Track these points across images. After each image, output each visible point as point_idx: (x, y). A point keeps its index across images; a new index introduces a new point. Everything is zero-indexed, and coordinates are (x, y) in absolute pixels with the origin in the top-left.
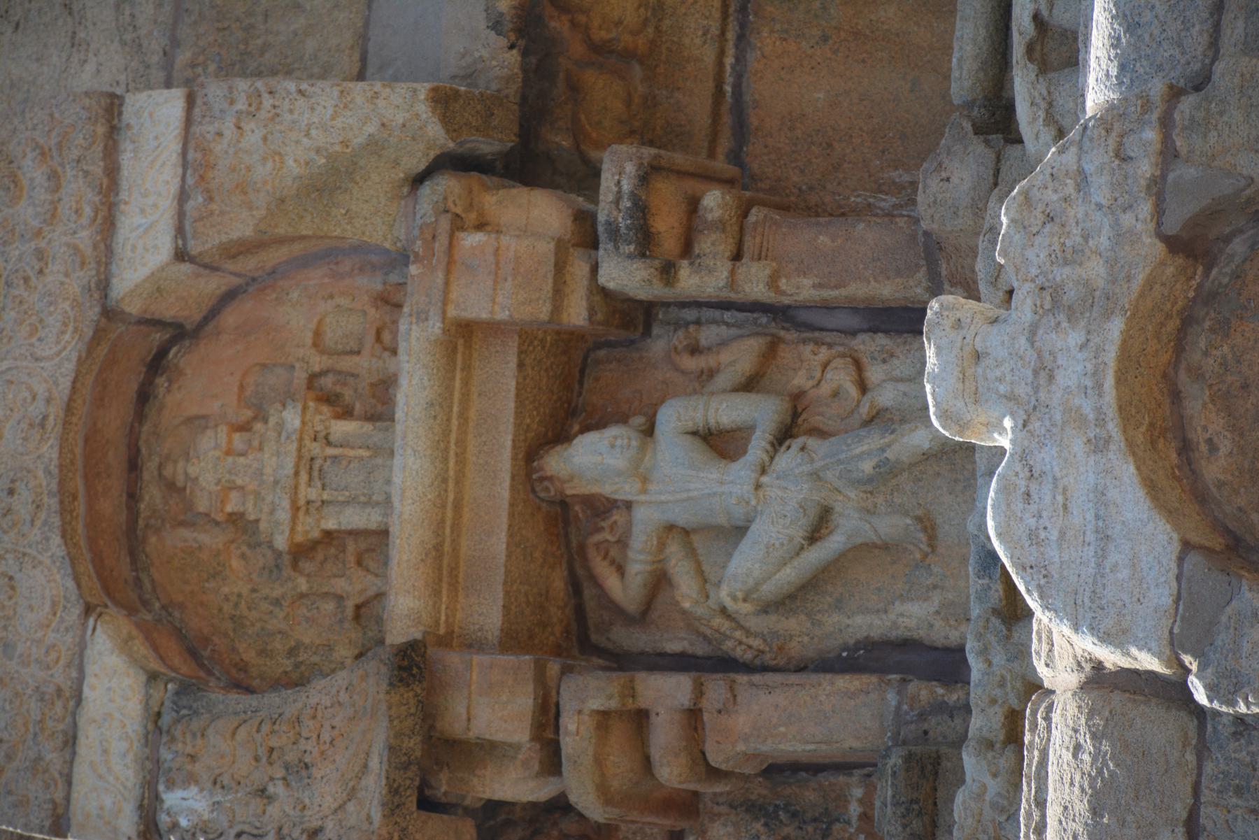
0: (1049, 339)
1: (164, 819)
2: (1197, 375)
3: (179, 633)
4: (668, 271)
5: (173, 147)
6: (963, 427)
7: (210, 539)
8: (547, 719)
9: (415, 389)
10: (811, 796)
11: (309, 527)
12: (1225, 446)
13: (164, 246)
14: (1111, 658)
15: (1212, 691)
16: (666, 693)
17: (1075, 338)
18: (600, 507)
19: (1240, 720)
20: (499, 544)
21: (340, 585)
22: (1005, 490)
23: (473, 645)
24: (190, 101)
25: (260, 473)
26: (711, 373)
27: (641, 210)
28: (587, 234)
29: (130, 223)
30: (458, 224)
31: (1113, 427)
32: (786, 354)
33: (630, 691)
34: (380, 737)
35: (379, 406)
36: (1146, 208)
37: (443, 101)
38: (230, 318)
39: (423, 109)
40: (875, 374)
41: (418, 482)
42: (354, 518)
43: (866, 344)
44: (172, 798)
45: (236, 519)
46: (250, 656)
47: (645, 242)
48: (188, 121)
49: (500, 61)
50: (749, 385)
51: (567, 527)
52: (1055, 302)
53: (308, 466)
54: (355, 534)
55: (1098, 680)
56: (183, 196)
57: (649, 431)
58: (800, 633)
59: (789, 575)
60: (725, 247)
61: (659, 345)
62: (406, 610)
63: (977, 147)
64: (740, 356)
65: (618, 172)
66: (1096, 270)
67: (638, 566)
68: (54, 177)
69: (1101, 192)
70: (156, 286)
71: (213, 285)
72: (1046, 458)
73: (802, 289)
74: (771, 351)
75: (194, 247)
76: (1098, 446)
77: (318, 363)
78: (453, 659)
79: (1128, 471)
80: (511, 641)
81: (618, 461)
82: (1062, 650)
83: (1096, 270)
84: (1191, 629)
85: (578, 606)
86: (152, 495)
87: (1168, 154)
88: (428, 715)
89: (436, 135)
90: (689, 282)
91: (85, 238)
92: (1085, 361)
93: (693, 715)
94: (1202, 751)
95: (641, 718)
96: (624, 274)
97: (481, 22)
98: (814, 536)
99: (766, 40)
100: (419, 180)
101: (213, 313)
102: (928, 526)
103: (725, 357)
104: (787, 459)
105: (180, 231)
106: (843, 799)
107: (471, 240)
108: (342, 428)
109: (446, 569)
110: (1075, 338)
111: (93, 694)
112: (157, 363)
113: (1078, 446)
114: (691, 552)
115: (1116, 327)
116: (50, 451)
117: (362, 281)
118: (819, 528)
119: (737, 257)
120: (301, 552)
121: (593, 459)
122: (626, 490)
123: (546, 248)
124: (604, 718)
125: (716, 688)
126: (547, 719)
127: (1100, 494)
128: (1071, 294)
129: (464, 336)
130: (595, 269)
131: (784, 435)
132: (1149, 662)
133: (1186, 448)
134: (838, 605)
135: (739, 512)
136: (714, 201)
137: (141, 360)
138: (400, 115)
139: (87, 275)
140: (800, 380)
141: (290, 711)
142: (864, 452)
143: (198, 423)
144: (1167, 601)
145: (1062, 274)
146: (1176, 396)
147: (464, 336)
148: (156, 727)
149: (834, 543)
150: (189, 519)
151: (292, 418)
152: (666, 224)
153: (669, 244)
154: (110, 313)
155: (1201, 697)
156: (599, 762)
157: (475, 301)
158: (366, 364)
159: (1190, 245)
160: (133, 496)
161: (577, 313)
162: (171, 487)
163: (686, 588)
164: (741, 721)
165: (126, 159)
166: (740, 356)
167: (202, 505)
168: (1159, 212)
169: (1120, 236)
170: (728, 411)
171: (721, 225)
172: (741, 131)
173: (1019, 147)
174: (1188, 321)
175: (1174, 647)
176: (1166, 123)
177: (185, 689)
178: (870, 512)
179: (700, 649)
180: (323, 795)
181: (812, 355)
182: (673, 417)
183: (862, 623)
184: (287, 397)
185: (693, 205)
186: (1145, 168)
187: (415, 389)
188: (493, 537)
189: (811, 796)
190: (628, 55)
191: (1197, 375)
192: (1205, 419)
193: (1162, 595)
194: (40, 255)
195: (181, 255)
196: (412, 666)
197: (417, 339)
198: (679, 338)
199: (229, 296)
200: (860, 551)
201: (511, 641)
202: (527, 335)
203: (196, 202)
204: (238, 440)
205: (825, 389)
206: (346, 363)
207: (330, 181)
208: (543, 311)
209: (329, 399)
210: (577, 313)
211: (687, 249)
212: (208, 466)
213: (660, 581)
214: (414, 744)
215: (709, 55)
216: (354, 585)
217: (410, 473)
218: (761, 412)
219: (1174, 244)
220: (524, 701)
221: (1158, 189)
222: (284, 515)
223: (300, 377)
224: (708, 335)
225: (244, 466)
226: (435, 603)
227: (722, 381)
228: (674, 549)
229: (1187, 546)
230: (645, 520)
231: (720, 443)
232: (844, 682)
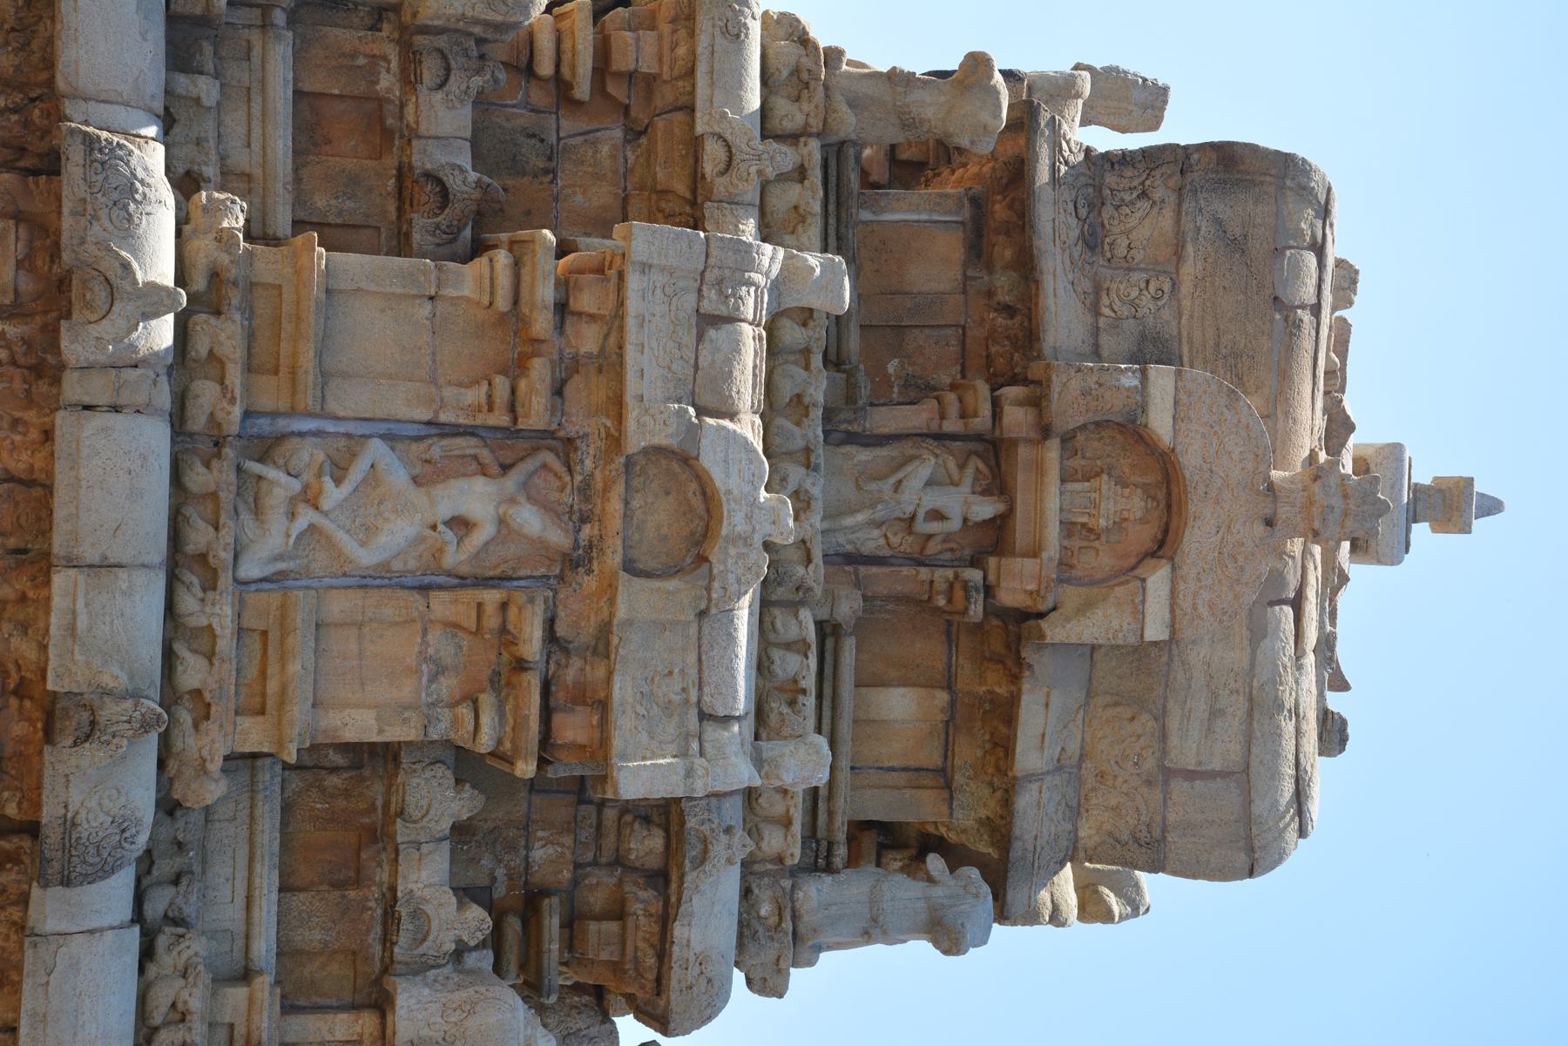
0: (748, 528)
1: (1138, 375)
2: (701, 518)
3: (1147, 445)
4: (956, 576)
5: (1148, 619)
6: (779, 500)
7: (1136, 479)
8: (997, 414)
9: (1053, 533)
10: (912, 394)
11: (1094, 483)
12: (690, 494)
13: (1150, 584)
14: (726, 423)
15: (687, 411)
16: (952, 425)
17: (739, 528)
18: (986, 492)
19: (679, 402)
20: (1020, 477)
21: (1083, 462)
22: (762, 478)
23: (1029, 441)
24: (1142, 636)
25: (1116, 503)
26: (944, 541)
27: (967, 598)
28: (989, 590)
29: (1164, 591)
30: (1038, 592)
31: (724, 498)
32: (917, 548)
33: (966, 425)
34: (1054, 406)
35: (1068, 528)
36: (715, 571)
37: (1042, 636)
38: (1133, 561)
39: (1048, 632)
40: (882, 541)
41: (1048, 501)
42: (1077, 486)
43: (886, 552)
44: (1136, 382)
45: (1125, 485)
46: (1118, 436)
47: (966, 586)
48: (1142, 629)
49: (1027, 654)
50: (930, 537)
51: (998, 484)
52: (746, 540)
53: (1096, 506)
54: (1078, 481)
55: (732, 415)
56: (1143, 602)
57: (965, 520)
58: (907, 448)
59: (909, 468)
60: (936, 585)
61: (967, 552)
62: (1052, 452)
63: (840, 619)
64: (933, 547)
65: (976, 610)
66: (732, 551)
67: (970, 471)
68: (1195, 608)
69: (731, 578)
70: (1154, 569)
71: (1137, 572)
72: (747, 488)
73: (906, 571)
74: (923, 548)
75: (1139, 583)
76: (729, 492)
77: (1097, 544)
78: (1033, 435)
79: (718, 484)
80: (1014, 443)
81: (975, 508)
82: (749, 428)
83: (732, 551)
84: (694, 432)
85: (993, 457)
86: (1161, 495)
87: (708, 589)
88: (1040, 415)
89: (1044, 624)
90: (950, 573)
91: (1182, 586)
92: (734, 520)
93: (942, 417)
94: (693, 393)
95: (963, 415)
96: (975, 575)
97: (1036, 667)
98: (900, 481)
99: (941, 666)
100: (1054, 609)
101: (1139, 562)
102: (859, 487)
103: (939, 547)
104: (910, 509)
105: (1144, 589)
106: (900, 393)
107: (1032, 587)
108: (1084, 519)
109: (1039, 468)
110: (739, 528)
111: (1168, 420)
112: (1161, 544)
113: (736, 492)
114: (950, 477)
115: (724, 532)
116: (1192, 508)
117: (1080, 574)
118: (898, 485)
119: (932, 582)
120: (1098, 475)
121: (985, 509)
122: (973, 498)
123: (1003, 584)
124: (976, 415)
125: (934, 427)
126: (997, 414)
127: (728, 476)
128: (741, 543)
129: (1035, 554)
130: (985, 578)
131: (913, 518)
132: (710, 421)
133: (704, 493)
134: (893, 459)
135: (928, 490)
136: (941, 602)
137: (1163, 545)
138: (1055, 631)
139: (1179, 573)
140: (910, 539)
141: (1090, 414)
142: (880, 513)
143: (1142, 521)
144: (703, 441)
145: (745, 550)
146: (708, 511)
147: (1035, 554)
148: (1144, 408)
149: (892, 480)
150: (1145, 487)
151: (1103, 523)
152: (959, 594)
153: (957, 587)
154: (1172, 559)
155: (691, 410)
156: (976, 400)
157: (1029, 565)
158: (1076, 543)
159: (702, 559)
160: (1169, 494)
161: (992, 561)
162: (1154, 499)
163: (952, 464)
164: (925, 416)
165: (1168, 615)
166: (933, 547)
167: (1139, 491)
168: (711, 570)
169: (724, 562)
170: (935, 527)
171: (938, 593)
172: (948, 633)
173: (819, 618)
174: (705, 536)
175: (700, 426)
176: (710, 600)
177: (1133, 422)
178: (879, 491)
179: (948, 443)
180: (1075, 384)
181: (906, 548)
182: (955, 524)
183: (883, 452)
184: (1107, 530)
185: (950, 601)
186: (716, 585)
187: (1053, 533)
188: (1022, 480)
189: (912, 394)
190: (990, 660)
191: (701, 518)
192: (697, 503)
193: (705, 442)
194: (1199, 580)
195: (1144, 580)
196: (1045, 432)
197: (1052, 550)
198: (958, 554)
199: (1133, 568)
200: (882, 478)
201: (1014, 443)
202: (1013, 554)
203: (1138, 599)
204: (1126, 515)
205: (900, 536)
206: (1085, 543)
207: (1085, 608)
208: (1003, 561)
209: (1091, 530)
210: (992, 561)
211: (951, 586)
212: (1136, 505)
213: (962, 467)
214: (1044, 404)
215: (961, 660)
216: (1077, 463)
217: (1053, 502)
218: (922, 527)
219: (706, 559)
220: (1006, 420)
221: (711, 578)
222: (1104, 487)
223: (1103, 538)
224: (948, 556)
225: (1120, 504)
226: (55, 251)
227: (939, 539)
228: (956, 478)
229: (697, 458)
230: (966, 488)
231: (937, 515)
232: (886, 430)
